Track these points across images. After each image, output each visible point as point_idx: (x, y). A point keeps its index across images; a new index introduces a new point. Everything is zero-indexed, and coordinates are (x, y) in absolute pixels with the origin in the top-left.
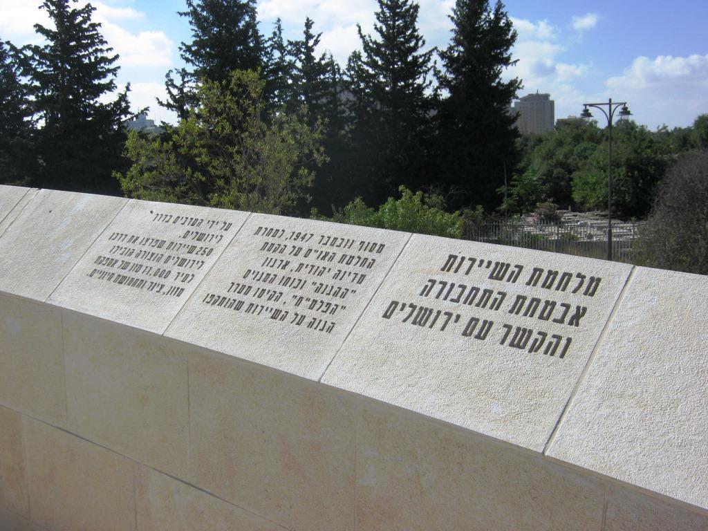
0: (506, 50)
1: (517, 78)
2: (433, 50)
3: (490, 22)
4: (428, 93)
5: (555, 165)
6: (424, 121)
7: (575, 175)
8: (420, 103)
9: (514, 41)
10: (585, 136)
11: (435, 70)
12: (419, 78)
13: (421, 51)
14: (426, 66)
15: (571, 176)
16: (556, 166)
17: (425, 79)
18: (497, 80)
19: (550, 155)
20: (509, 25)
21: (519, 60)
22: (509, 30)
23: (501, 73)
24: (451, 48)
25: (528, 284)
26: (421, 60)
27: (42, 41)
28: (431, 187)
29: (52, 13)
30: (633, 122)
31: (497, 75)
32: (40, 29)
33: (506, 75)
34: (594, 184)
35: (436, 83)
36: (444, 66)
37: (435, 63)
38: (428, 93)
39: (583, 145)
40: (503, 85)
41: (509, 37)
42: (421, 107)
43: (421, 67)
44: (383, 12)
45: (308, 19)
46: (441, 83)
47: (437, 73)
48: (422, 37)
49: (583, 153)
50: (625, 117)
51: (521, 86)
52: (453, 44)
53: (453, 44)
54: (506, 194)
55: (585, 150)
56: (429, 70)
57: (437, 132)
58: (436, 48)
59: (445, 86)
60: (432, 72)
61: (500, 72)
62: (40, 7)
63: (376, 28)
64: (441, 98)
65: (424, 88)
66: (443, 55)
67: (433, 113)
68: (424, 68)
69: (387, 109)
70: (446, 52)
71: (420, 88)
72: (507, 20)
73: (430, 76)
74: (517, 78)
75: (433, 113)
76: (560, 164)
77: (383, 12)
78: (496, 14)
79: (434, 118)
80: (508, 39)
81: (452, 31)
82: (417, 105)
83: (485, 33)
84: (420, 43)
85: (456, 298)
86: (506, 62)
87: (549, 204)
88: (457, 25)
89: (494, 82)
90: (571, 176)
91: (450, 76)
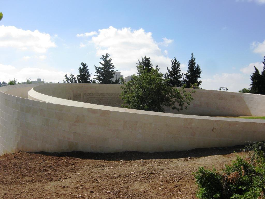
13: (181, 73)
24: (187, 73)
27: (102, 66)
29: (103, 60)
32: (101, 63)
44: (173, 65)
45: (157, 65)
61: (197, 79)
62: (95, 66)
63: (171, 68)
66: (185, 75)
77: (173, 65)
78: (197, 67)
86: (199, 77)
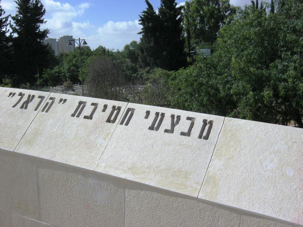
0: (42, 17)
1: (47, 29)
2: (9, 16)
3: (34, 4)
4: (8, 35)
5: (72, 66)
6: (7, 47)
7: (80, 69)
8: (4, 39)
9: (45, 13)
10: (85, 53)
11: (10, 25)
12: (3, 28)
14: (6, 23)
15: (79, 70)
16: (72, 66)
17: (6, 29)
18: (38, 30)
19: (71, 61)
20: (42, 6)
21: (47, 21)
22: (42, 8)
23: (40, 26)
24: (17, 15)
25: (73, 115)
26: (4, 20)
28: (6, 76)
30: (88, 46)
31: (38, 28)
33: (42, 27)
34: (87, 73)
35: (11, 31)
36: (14, 23)
37: (10, 21)
38: (8, 35)
39: (83, 57)
40: (41, 32)
41: (42, 11)
42: (5, 41)
43: (4, 23)
46: (14, 31)
47: (11, 26)
48: (3, 10)
49: (83, 61)
50: (85, 45)
51: (49, 32)
52: (18, 13)
53: (18, 14)
54: (265, 72)
55: (84, 59)
56: (8, 24)
57: (13, 52)
58: (10, 15)
59: (16, 32)
60: (9, 26)
61: (39, 26)
64: (13, 37)
65: (6, 33)
66: (14, 18)
67: (11, 44)
68: (5, 24)
69: (254, 23)
70: (15, 17)
71: (4, 33)
72: (41, 4)
73: (8, 27)
74: (47, 29)
75: (11, 44)
76: (74, 65)
79: (11, 46)
80: (42, 12)
81: (16, 8)
82: (3, 40)
83: (31, 9)
84: (3, 12)
85: (186, 131)
86: (42, 22)
87: (69, 82)
88: (19, 5)
89: (37, 31)
90: (79, 70)
91: (17, 28)
